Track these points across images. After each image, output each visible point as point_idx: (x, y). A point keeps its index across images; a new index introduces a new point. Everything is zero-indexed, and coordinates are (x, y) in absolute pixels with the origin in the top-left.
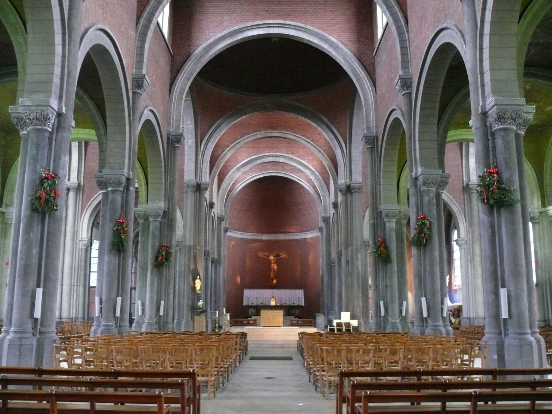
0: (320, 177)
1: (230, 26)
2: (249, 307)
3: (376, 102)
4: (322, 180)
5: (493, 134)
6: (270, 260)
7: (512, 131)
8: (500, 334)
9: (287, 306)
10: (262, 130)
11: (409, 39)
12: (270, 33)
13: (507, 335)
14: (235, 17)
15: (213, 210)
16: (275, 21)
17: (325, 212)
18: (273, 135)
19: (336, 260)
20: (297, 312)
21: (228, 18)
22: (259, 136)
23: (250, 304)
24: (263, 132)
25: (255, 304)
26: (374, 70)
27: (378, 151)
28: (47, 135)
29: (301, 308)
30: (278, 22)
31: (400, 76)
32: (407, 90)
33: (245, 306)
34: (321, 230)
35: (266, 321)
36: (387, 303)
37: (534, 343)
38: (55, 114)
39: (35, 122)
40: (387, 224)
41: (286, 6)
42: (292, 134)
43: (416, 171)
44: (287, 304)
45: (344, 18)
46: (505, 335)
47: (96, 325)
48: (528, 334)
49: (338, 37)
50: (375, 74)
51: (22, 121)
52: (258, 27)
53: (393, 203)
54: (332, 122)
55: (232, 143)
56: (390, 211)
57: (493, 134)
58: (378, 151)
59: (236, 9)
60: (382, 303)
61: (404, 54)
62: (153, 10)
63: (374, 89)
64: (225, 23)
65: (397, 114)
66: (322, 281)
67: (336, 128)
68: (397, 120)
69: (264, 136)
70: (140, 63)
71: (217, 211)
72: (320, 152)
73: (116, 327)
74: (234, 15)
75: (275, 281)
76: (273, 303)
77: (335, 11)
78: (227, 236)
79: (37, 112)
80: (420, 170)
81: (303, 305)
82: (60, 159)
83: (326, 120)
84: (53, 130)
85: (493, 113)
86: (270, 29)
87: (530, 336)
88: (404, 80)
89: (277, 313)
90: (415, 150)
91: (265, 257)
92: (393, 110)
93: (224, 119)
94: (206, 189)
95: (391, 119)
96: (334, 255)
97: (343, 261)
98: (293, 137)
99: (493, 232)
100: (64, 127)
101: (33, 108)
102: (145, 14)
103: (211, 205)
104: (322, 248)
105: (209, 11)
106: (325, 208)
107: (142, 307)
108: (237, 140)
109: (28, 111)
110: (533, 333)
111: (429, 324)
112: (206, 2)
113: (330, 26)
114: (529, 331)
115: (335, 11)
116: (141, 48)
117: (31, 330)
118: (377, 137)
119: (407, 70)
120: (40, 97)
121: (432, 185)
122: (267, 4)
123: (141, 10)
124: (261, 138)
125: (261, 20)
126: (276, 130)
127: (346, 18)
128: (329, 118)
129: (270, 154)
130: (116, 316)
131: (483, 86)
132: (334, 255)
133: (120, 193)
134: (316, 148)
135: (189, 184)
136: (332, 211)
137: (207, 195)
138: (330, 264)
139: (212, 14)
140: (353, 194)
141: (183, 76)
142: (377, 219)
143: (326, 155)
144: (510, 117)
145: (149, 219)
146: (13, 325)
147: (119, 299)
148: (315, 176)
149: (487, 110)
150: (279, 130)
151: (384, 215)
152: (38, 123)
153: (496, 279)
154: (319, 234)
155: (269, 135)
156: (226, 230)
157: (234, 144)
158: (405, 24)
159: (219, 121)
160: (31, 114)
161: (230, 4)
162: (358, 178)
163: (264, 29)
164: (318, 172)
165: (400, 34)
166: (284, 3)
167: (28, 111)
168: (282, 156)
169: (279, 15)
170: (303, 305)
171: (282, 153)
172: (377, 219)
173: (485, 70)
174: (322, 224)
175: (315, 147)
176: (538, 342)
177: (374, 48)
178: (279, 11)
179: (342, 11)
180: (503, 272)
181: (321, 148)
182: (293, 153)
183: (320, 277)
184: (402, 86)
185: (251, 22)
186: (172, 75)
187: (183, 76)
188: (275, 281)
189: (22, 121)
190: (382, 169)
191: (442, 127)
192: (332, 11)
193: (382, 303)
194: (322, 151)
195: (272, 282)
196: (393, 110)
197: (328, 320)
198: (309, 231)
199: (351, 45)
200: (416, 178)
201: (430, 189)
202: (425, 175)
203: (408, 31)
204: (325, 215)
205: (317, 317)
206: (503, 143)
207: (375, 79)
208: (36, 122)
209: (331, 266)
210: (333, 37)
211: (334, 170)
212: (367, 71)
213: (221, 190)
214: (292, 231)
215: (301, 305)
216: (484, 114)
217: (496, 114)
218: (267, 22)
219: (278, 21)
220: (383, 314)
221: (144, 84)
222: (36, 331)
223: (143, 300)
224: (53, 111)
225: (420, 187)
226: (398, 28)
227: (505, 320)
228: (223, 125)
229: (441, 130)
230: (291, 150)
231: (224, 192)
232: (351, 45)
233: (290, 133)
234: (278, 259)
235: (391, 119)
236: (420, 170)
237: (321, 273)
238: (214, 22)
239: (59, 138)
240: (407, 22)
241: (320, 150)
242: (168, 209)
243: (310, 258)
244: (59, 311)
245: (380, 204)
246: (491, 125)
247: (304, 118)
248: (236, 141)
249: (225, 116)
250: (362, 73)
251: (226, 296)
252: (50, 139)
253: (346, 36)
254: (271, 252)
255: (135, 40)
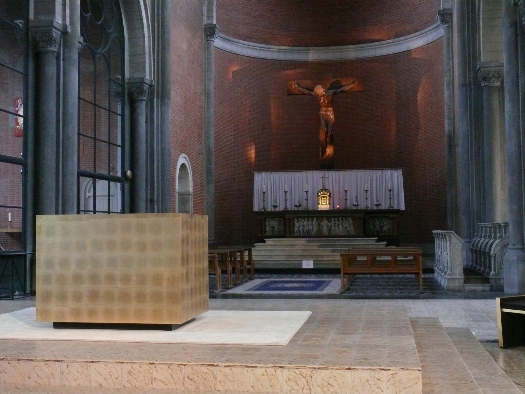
2: (265, 215)
6: (317, 97)
9: (360, 211)
20: (386, 226)
23: (269, 209)
25: (281, 208)
29: (395, 216)
33: (259, 213)
35: (71, 288)
44: (362, 207)
66: (451, 147)
75: (329, 151)
76: (324, 205)
78: (212, 48)
81: (403, 207)
89: (141, 229)
91: (306, 91)
154: (441, 32)
170: (403, 207)
183: (446, 139)
188: (329, 151)
195: (324, 152)
197: (472, 250)
198: (417, 31)
205: (437, 242)
209: (478, 88)
214: (377, 37)
215: (396, 208)
234: (335, 94)
237: (447, 128)
243: (420, 96)
251: (212, 190)
254: (319, 81)
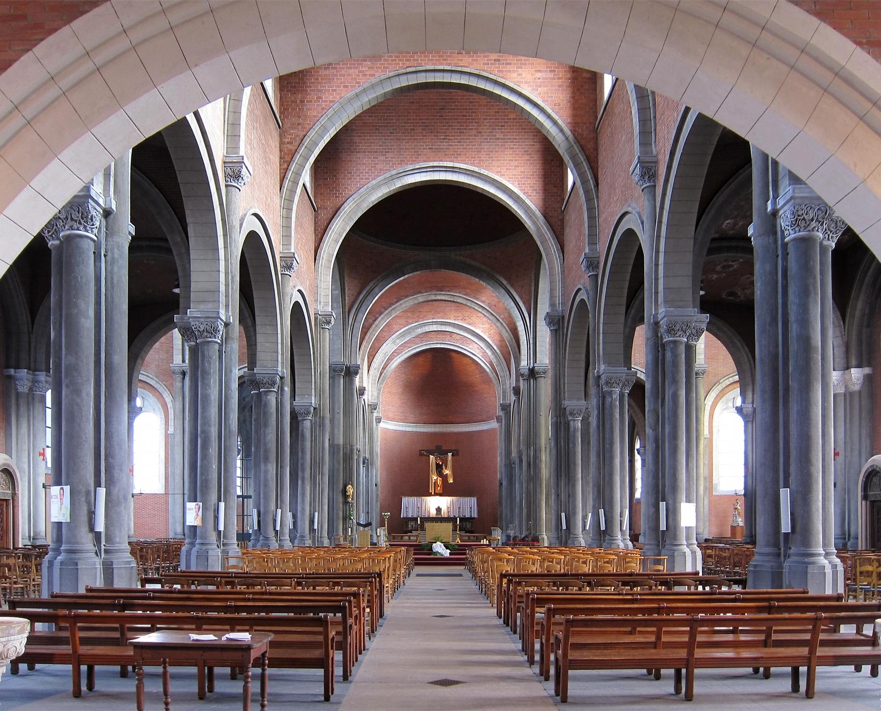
0: (498, 351)
1: (386, 170)
2: (408, 520)
3: (563, 272)
4: (500, 355)
5: (663, 346)
7: (682, 343)
8: (658, 546)
10: (423, 291)
11: (598, 206)
12: (435, 179)
13: (664, 546)
14: (391, 158)
15: (364, 397)
16: (441, 164)
17: (504, 397)
18: (439, 297)
19: (517, 461)
21: (383, 158)
22: (421, 300)
24: (425, 294)
26: (563, 228)
27: (563, 334)
28: (217, 347)
30: (445, 165)
31: (585, 254)
32: (593, 271)
34: (499, 419)
36: (569, 514)
37: (828, 570)
38: (223, 324)
39: (205, 334)
40: (572, 423)
41: (455, 142)
42: (463, 296)
43: (599, 368)
45: (528, 157)
46: (785, 556)
47: (256, 540)
48: (819, 555)
49: (519, 184)
50: (563, 235)
51: (188, 331)
52: (420, 170)
53: (579, 399)
54: (512, 285)
55: (386, 309)
56: (575, 407)
57: (663, 346)
58: (563, 334)
59: (394, 146)
60: (563, 515)
61: (592, 226)
62: (299, 169)
63: (562, 255)
64: (379, 166)
65: (582, 295)
67: (517, 293)
68: (582, 300)
69: (426, 300)
70: (287, 237)
71: (368, 397)
72: (499, 320)
73: (277, 541)
74: (390, 155)
77: (516, 148)
79: (207, 324)
80: (602, 367)
81: (476, 516)
82: (231, 371)
83: (505, 282)
84: (222, 341)
85: (663, 323)
86: (435, 173)
87: (822, 558)
88: (589, 259)
90: (599, 344)
92: (579, 290)
93: (378, 280)
94: (356, 373)
95: (578, 300)
96: (514, 454)
97: (524, 464)
98: (464, 300)
99: (657, 447)
100: (232, 338)
101: (203, 320)
102: (289, 175)
103: (362, 391)
104: (500, 444)
105: (359, 149)
106: (504, 392)
107: (292, 520)
108: (393, 304)
109: (197, 323)
110: (827, 555)
111: (792, 551)
112: (355, 136)
113: (510, 169)
114: (685, 542)
115: (516, 148)
116: (288, 218)
117: (236, 542)
118: (563, 317)
119: (594, 246)
120: (209, 306)
121: (615, 385)
122: (431, 139)
123: (284, 169)
124: (423, 302)
125: (425, 161)
126: (442, 291)
127: (530, 157)
128: (509, 279)
129: (434, 320)
130: (97, 530)
131: (657, 293)
132: (514, 454)
133: (274, 394)
134: (493, 315)
135: (336, 367)
136: (513, 398)
137: (357, 379)
138: (509, 466)
139: (363, 152)
140: (538, 379)
141: (330, 237)
142: (560, 416)
143: (505, 325)
144: (680, 329)
145: (297, 418)
146: (198, 537)
147: (279, 511)
148: (491, 350)
149: (659, 320)
150: (446, 291)
151: (568, 412)
152: (209, 336)
153: (657, 493)
155: (433, 298)
156: (379, 420)
157: (389, 310)
158: (595, 187)
159: (371, 284)
160: (201, 326)
161: (385, 139)
162: (544, 358)
163: (428, 173)
164: (495, 345)
165: (589, 200)
166: (452, 138)
167: (197, 323)
168: (449, 324)
169: (446, 155)
171: (450, 319)
172: (560, 416)
173: (660, 277)
174: (499, 413)
175: (492, 314)
176: (834, 567)
177: (564, 200)
178: (446, 149)
179: (525, 148)
180: (664, 486)
181: (499, 315)
182: (463, 319)
184: (588, 267)
185: (411, 164)
186: (316, 235)
187: (330, 237)
189: (188, 331)
190: (567, 356)
191: (631, 316)
192: (513, 148)
193: (563, 515)
194: (500, 320)
196: (579, 290)
199: (535, 196)
200: (599, 377)
201: (613, 389)
202: (607, 374)
203: (597, 197)
204: (504, 402)
206: (672, 356)
207: (563, 241)
208: (206, 334)
209: (511, 467)
210: (513, 184)
211: (515, 345)
212: (554, 232)
213: (372, 369)
216: (657, 324)
217: (666, 326)
218: (431, 164)
219: (445, 164)
220: (564, 527)
221: (294, 265)
222: (220, 543)
223: (294, 513)
224: (221, 322)
225: (602, 387)
226: (587, 192)
227: (786, 534)
228: (376, 289)
229: (630, 320)
230: (460, 315)
231: (376, 371)
232: (535, 196)
233: (461, 295)
235: (578, 300)
236: (602, 367)
238: (365, 164)
239: (228, 349)
240: (597, 185)
241: (499, 318)
242: (320, 405)
244: (182, 526)
245: (565, 399)
246: (662, 337)
247: (477, 280)
248: (390, 306)
249: (379, 278)
250: (547, 234)
252: (220, 351)
253: (528, 184)
255: (280, 209)
